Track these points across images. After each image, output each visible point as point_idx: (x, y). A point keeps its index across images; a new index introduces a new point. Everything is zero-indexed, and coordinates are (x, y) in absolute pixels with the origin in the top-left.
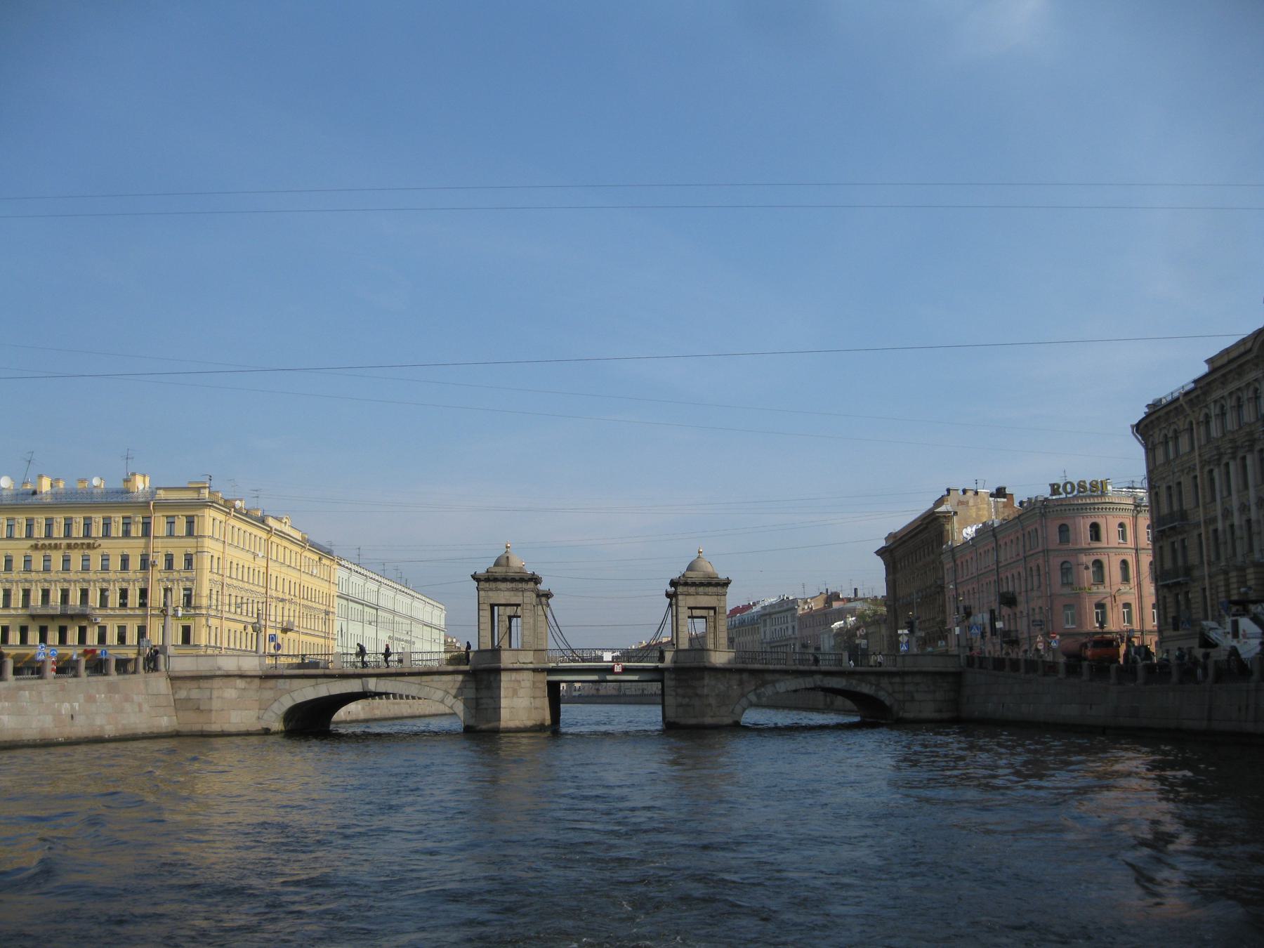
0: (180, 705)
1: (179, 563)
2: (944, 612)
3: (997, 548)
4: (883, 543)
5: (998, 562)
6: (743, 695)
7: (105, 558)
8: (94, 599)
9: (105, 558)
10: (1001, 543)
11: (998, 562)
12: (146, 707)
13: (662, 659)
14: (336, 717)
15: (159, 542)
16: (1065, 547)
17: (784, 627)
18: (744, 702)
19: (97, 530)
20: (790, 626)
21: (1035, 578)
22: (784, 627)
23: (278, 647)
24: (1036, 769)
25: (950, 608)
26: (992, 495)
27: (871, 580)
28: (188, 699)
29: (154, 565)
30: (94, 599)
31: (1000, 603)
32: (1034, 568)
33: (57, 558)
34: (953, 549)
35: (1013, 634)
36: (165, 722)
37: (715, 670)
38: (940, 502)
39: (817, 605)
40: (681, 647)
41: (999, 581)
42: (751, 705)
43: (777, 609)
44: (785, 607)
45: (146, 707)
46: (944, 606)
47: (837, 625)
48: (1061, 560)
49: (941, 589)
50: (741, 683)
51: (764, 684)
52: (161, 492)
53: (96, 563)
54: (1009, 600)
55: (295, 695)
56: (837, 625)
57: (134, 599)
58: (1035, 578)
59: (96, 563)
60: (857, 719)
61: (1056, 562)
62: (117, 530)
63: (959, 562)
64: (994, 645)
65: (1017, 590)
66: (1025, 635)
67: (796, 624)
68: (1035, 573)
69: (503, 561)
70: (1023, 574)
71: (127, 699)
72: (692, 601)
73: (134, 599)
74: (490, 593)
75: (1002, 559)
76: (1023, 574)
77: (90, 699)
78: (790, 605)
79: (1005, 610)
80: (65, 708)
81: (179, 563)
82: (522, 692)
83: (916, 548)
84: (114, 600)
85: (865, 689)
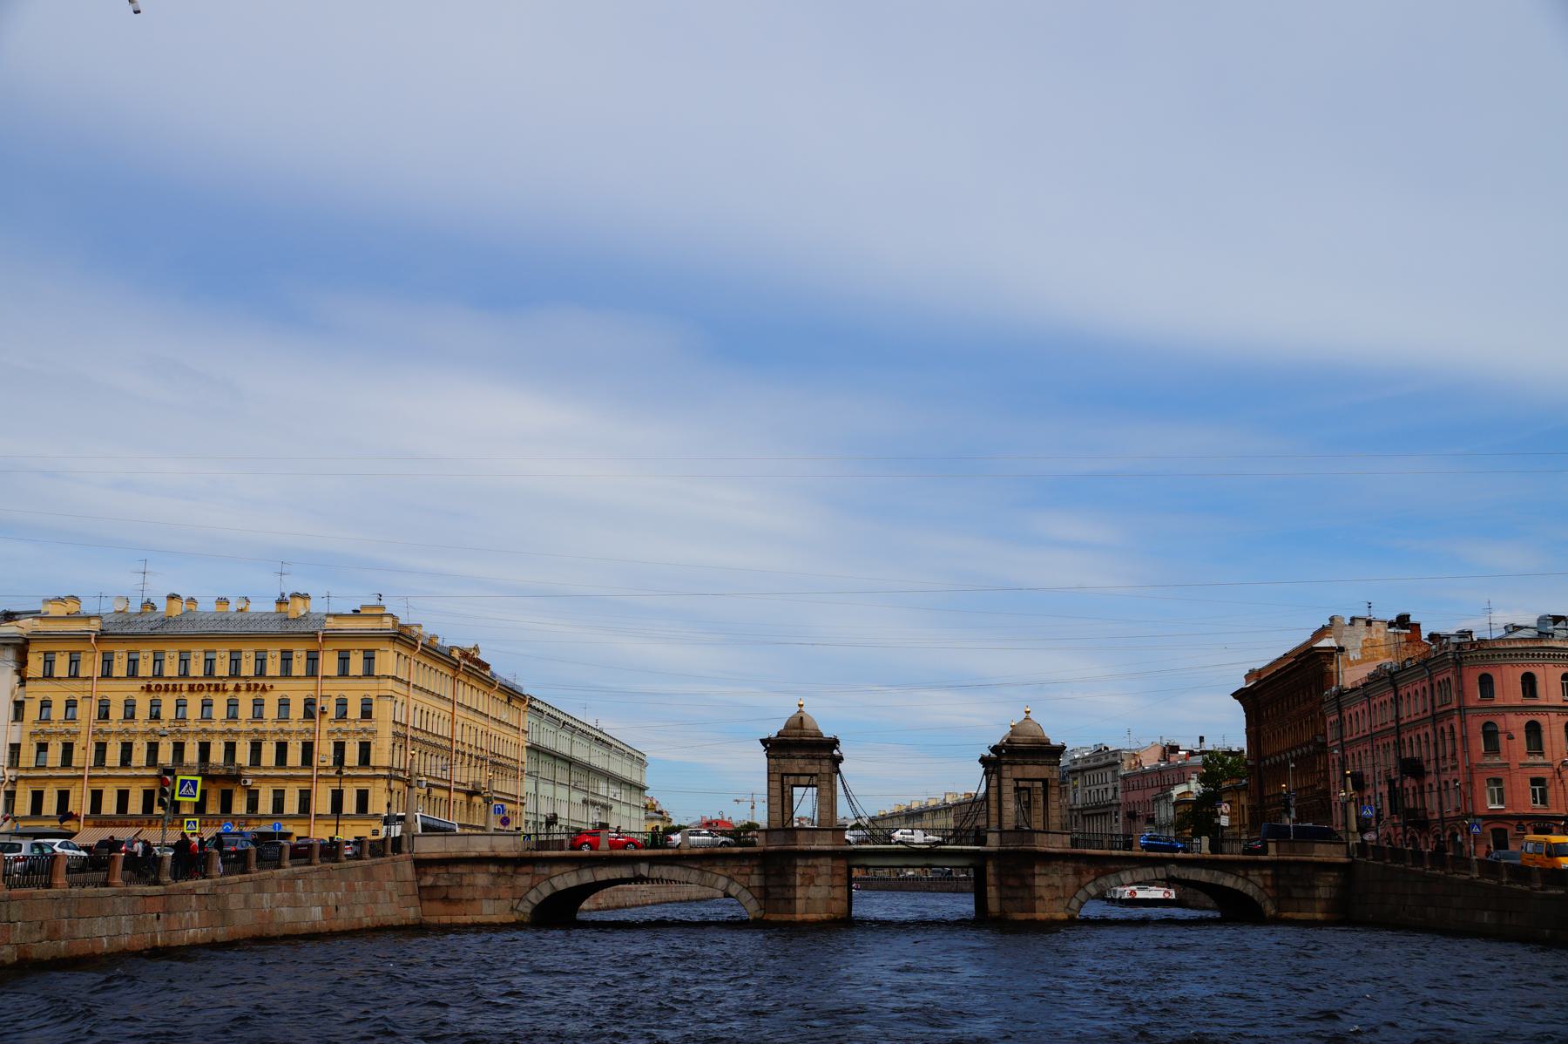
0: (425, 894)
1: (354, 711)
2: (1327, 780)
3: (1397, 701)
4: (1241, 683)
5: (1398, 719)
6: (1080, 887)
7: (284, 704)
8: (243, 756)
9: (284, 704)
10: (1403, 693)
11: (1398, 719)
12: (395, 898)
13: (983, 842)
14: (585, 905)
15: (327, 684)
16: (1486, 704)
17: (1102, 787)
18: (1081, 895)
19: (273, 668)
20: (1110, 785)
21: (1448, 745)
22: (1102, 787)
23: (505, 821)
24: (702, 872)
25: (1335, 776)
26: (1391, 625)
27: (1228, 729)
28: (434, 887)
29: (323, 711)
30: (243, 756)
31: (1402, 772)
32: (1447, 730)
33: (194, 702)
34: (1341, 692)
35: (1420, 813)
36: (411, 914)
37: (1048, 858)
38: (1321, 633)
39: (1150, 761)
40: (1006, 827)
41: (1399, 745)
42: (1091, 897)
43: (1092, 764)
44: (1104, 761)
45: (395, 898)
46: (1327, 771)
47: (1178, 790)
48: (1484, 720)
49: (1323, 748)
50: (1078, 873)
51: (1105, 874)
52: (330, 620)
53: (271, 710)
54: (1413, 768)
55: (555, 881)
56: (1178, 790)
57: (294, 756)
58: (1448, 745)
59: (271, 710)
60: (1218, 915)
61: (1475, 725)
62: (299, 667)
63: (1346, 714)
64: (1395, 826)
65: (1425, 758)
66: (1436, 816)
67: (1119, 784)
68: (1447, 737)
69: (798, 722)
70: (1432, 738)
71: (380, 888)
72: (1018, 772)
73: (294, 756)
74: (782, 762)
75: (1404, 713)
76: (1432, 738)
77: (351, 888)
78: (1111, 759)
79: (1410, 783)
80: (331, 898)
81: (354, 711)
82: (818, 881)
83: (1288, 694)
84: (269, 755)
85: (1229, 882)
